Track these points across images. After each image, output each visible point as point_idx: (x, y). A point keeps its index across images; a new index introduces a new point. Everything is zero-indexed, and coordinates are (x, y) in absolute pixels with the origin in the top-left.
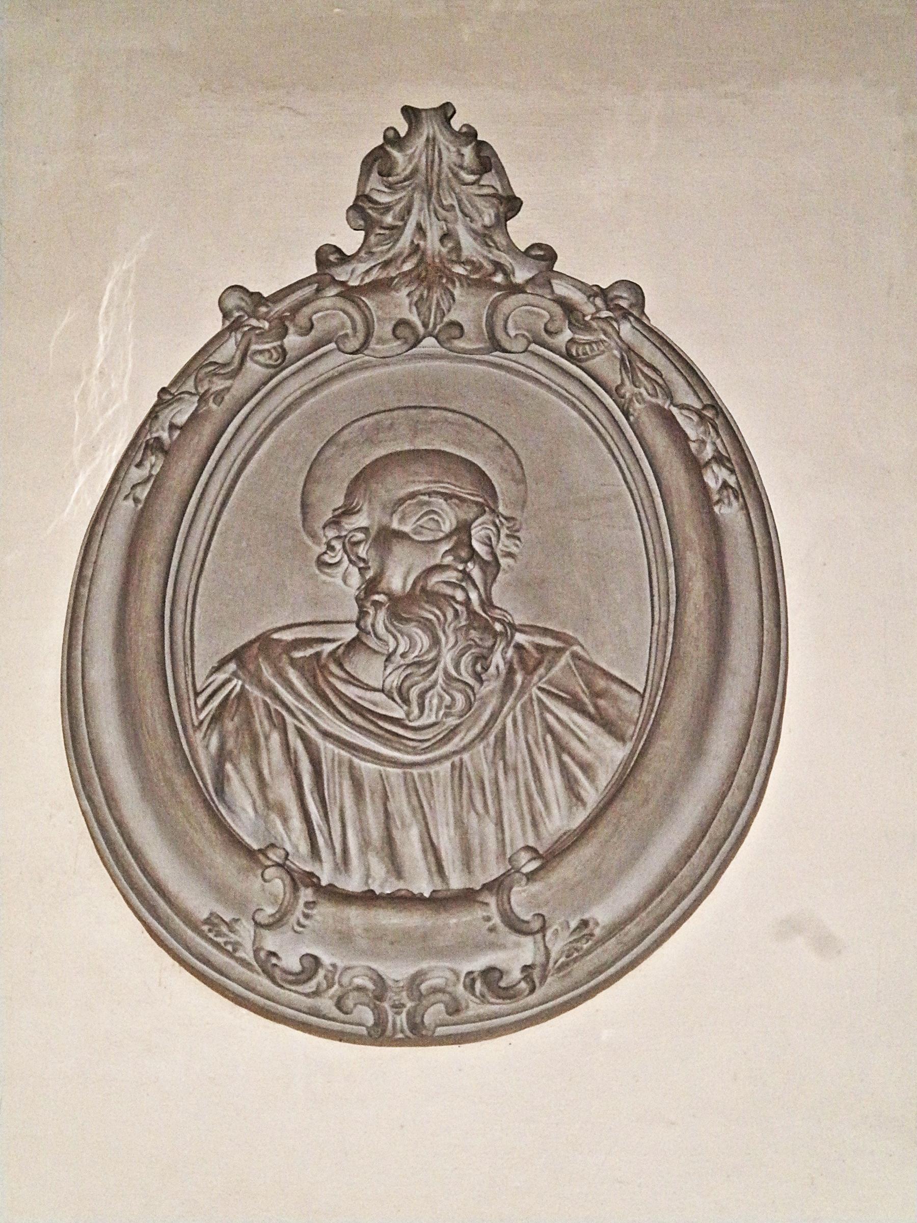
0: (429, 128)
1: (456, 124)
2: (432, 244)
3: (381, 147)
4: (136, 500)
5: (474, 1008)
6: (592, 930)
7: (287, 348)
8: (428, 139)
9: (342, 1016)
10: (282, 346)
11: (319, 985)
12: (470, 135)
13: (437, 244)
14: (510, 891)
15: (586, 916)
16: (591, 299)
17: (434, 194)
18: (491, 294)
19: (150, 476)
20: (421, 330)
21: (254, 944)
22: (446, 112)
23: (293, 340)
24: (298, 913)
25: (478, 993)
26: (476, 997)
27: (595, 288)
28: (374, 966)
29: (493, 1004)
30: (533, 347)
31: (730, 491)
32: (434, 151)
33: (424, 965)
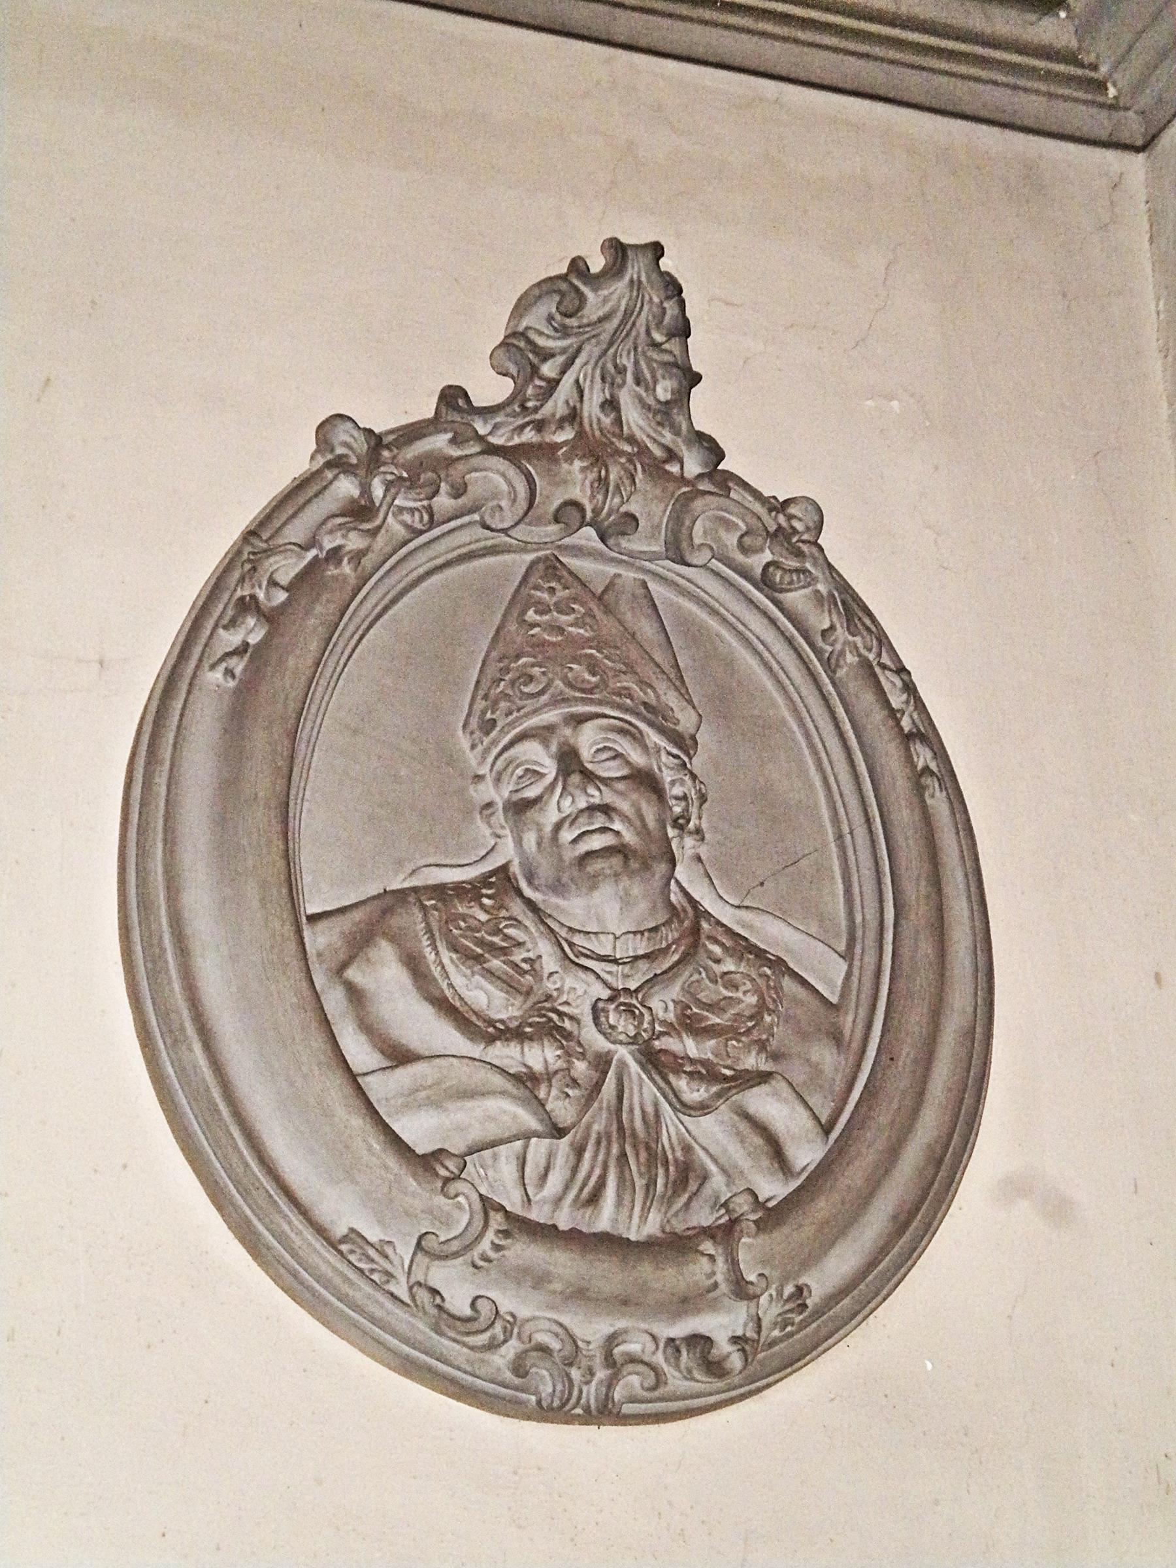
0: (637, 268)
1: (597, 264)
2: (591, 408)
3: (563, 278)
4: (229, 673)
5: (676, 1382)
6: (805, 1300)
7: (435, 509)
8: (632, 281)
9: (517, 1381)
10: (430, 506)
11: (493, 1338)
12: (673, 288)
13: (596, 411)
14: (739, 1241)
15: (801, 1281)
16: (773, 514)
17: (615, 347)
18: (679, 488)
19: (246, 645)
20: (589, 515)
21: (408, 1282)
22: (657, 250)
23: (443, 502)
24: (485, 1245)
25: (682, 1366)
26: (680, 1372)
27: (772, 500)
28: (565, 1320)
29: (698, 1381)
30: (716, 564)
31: (935, 779)
32: (638, 296)
33: (621, 1324)
